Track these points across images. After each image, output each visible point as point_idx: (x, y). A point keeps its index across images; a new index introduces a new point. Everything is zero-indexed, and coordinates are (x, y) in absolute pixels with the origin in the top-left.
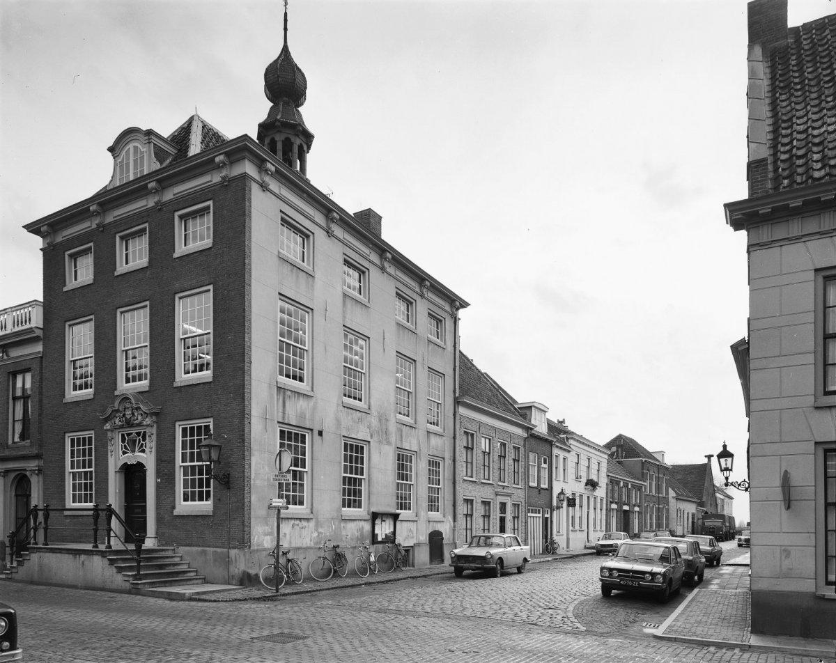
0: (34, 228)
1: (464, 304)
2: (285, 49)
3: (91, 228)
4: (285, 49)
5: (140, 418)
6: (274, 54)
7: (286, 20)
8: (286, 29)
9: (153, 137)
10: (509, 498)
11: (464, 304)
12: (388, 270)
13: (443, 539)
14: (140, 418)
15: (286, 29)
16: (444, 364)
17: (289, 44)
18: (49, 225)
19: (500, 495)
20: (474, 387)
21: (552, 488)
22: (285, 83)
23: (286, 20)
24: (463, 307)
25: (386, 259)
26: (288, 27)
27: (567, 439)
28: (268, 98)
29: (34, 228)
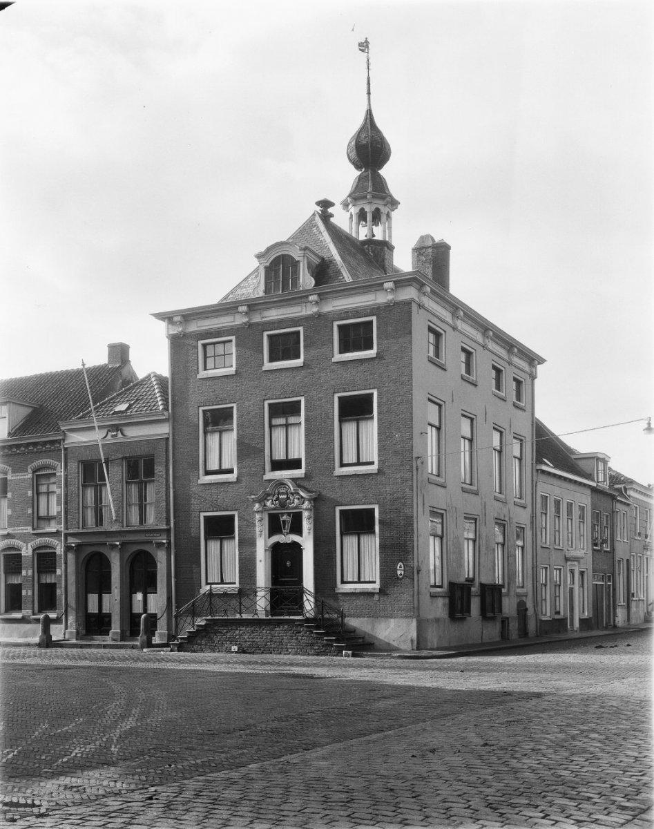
0: (168, 317)
1: (542, 361)
2: (369, 113)
3: (233, 324)
4: (369, 113)
5: (296, 501)
6: (358, 122)
7: (369, 84)
8: (369, 93)
9: (308, 252)
10: (576, 563)
11: (542, 361)
12: (490, 347)
13: (527, 609)
14: (296, 501)
15: (369, 93)
16: (527, 432)
17: (372, 107)
18: (183, 316)
19: (569, 560)
20: (548, 448)
21: (614, 550)
22: (370, 151)
23: (369, 84)
24: (539, 363)
25: (424, 294)
26: (371, 92)
27: (626, 489)
28: (350, 160)
29: (168, 317)
